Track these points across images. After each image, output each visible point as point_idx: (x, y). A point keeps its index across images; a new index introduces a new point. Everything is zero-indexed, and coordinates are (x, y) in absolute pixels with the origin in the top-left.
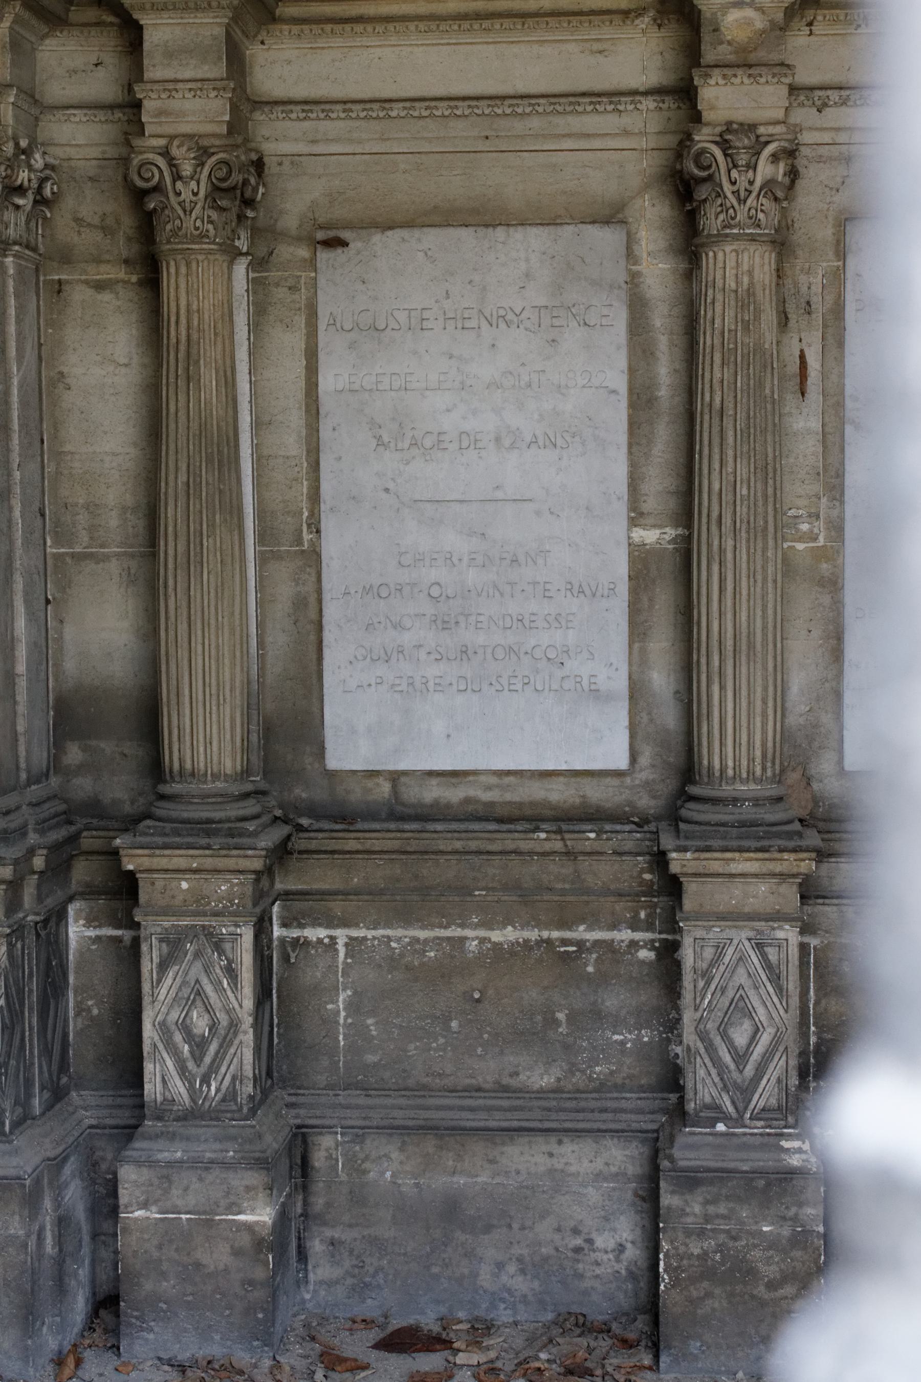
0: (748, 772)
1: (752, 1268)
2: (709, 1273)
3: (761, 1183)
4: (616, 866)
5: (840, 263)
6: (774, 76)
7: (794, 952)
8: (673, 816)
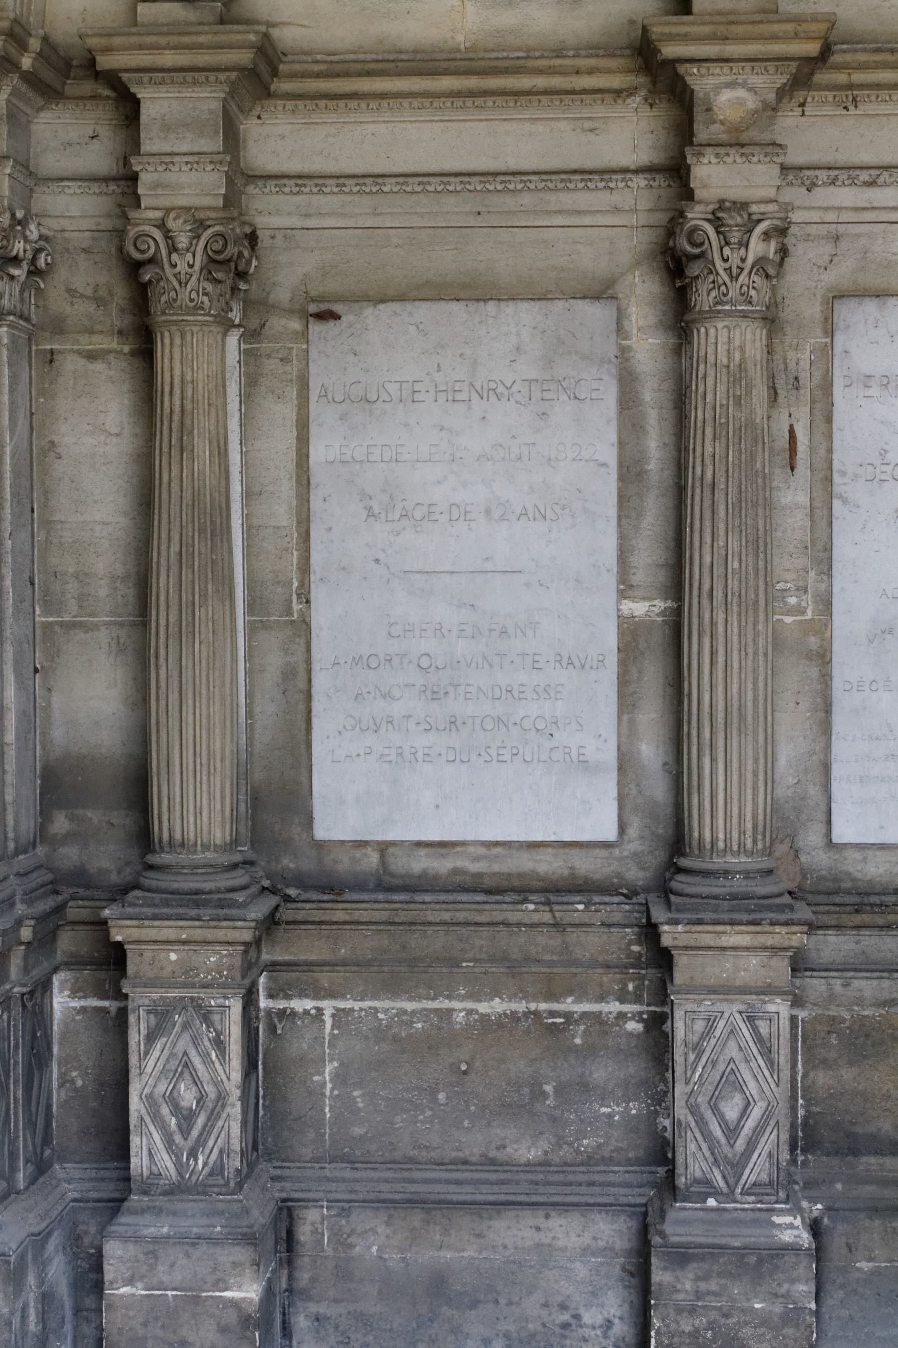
0: (739, 845)
3: (753, 1259)
5: (828, 340)
7: (785, 1025)
8: (665, 890)
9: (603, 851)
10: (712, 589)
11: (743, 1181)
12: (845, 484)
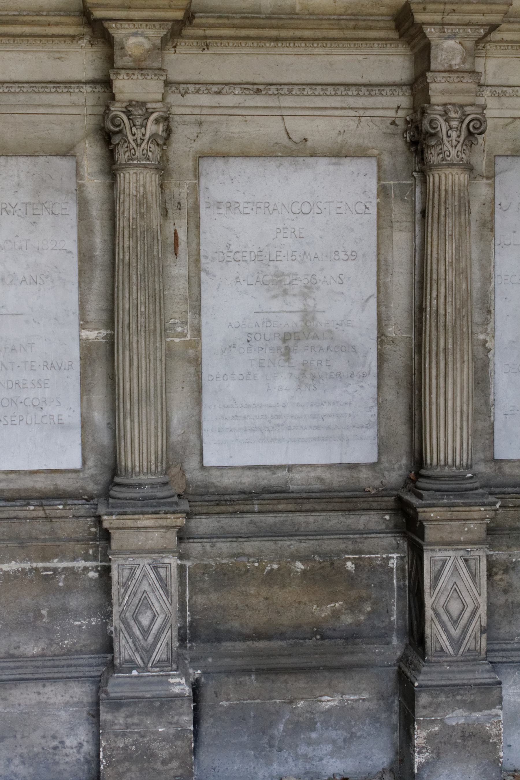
0: (147, 469)
1: (153, 753)
2: (129, 758)
3: (158, 703)
4: (75, 524)
5: (197, 181)
6: (155, 75)
7: (175, 571)
8: (106, 495)
9: (73, 474)
10: (129, 323)
11: (152, 660)
12: (207, 263)
